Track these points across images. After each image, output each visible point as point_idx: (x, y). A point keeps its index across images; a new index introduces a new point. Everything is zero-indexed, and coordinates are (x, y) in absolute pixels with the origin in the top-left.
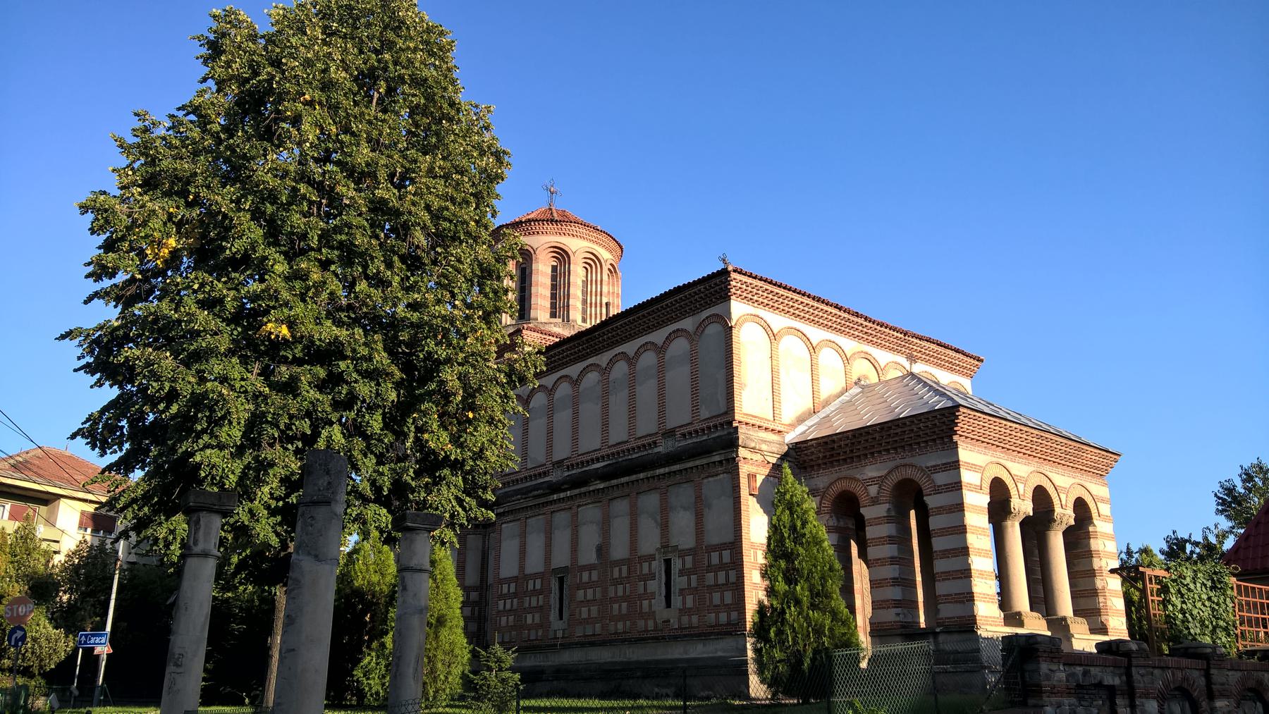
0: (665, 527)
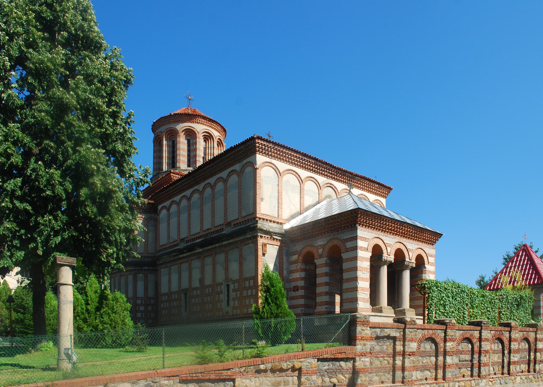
0: (227, 269)
